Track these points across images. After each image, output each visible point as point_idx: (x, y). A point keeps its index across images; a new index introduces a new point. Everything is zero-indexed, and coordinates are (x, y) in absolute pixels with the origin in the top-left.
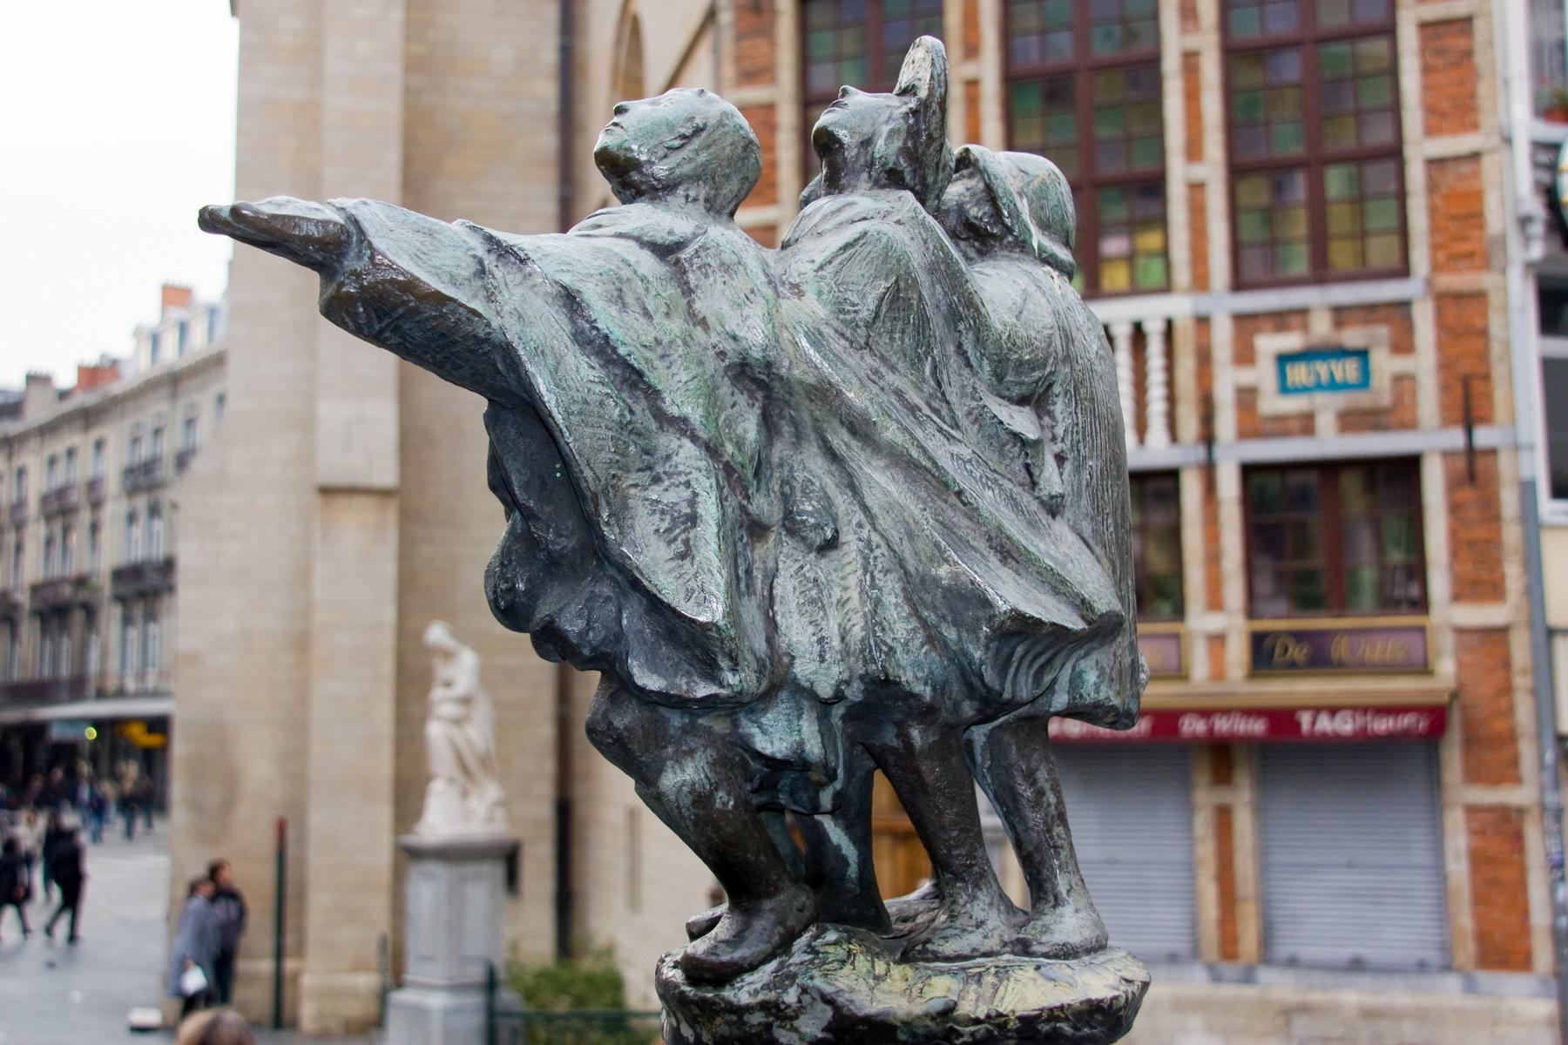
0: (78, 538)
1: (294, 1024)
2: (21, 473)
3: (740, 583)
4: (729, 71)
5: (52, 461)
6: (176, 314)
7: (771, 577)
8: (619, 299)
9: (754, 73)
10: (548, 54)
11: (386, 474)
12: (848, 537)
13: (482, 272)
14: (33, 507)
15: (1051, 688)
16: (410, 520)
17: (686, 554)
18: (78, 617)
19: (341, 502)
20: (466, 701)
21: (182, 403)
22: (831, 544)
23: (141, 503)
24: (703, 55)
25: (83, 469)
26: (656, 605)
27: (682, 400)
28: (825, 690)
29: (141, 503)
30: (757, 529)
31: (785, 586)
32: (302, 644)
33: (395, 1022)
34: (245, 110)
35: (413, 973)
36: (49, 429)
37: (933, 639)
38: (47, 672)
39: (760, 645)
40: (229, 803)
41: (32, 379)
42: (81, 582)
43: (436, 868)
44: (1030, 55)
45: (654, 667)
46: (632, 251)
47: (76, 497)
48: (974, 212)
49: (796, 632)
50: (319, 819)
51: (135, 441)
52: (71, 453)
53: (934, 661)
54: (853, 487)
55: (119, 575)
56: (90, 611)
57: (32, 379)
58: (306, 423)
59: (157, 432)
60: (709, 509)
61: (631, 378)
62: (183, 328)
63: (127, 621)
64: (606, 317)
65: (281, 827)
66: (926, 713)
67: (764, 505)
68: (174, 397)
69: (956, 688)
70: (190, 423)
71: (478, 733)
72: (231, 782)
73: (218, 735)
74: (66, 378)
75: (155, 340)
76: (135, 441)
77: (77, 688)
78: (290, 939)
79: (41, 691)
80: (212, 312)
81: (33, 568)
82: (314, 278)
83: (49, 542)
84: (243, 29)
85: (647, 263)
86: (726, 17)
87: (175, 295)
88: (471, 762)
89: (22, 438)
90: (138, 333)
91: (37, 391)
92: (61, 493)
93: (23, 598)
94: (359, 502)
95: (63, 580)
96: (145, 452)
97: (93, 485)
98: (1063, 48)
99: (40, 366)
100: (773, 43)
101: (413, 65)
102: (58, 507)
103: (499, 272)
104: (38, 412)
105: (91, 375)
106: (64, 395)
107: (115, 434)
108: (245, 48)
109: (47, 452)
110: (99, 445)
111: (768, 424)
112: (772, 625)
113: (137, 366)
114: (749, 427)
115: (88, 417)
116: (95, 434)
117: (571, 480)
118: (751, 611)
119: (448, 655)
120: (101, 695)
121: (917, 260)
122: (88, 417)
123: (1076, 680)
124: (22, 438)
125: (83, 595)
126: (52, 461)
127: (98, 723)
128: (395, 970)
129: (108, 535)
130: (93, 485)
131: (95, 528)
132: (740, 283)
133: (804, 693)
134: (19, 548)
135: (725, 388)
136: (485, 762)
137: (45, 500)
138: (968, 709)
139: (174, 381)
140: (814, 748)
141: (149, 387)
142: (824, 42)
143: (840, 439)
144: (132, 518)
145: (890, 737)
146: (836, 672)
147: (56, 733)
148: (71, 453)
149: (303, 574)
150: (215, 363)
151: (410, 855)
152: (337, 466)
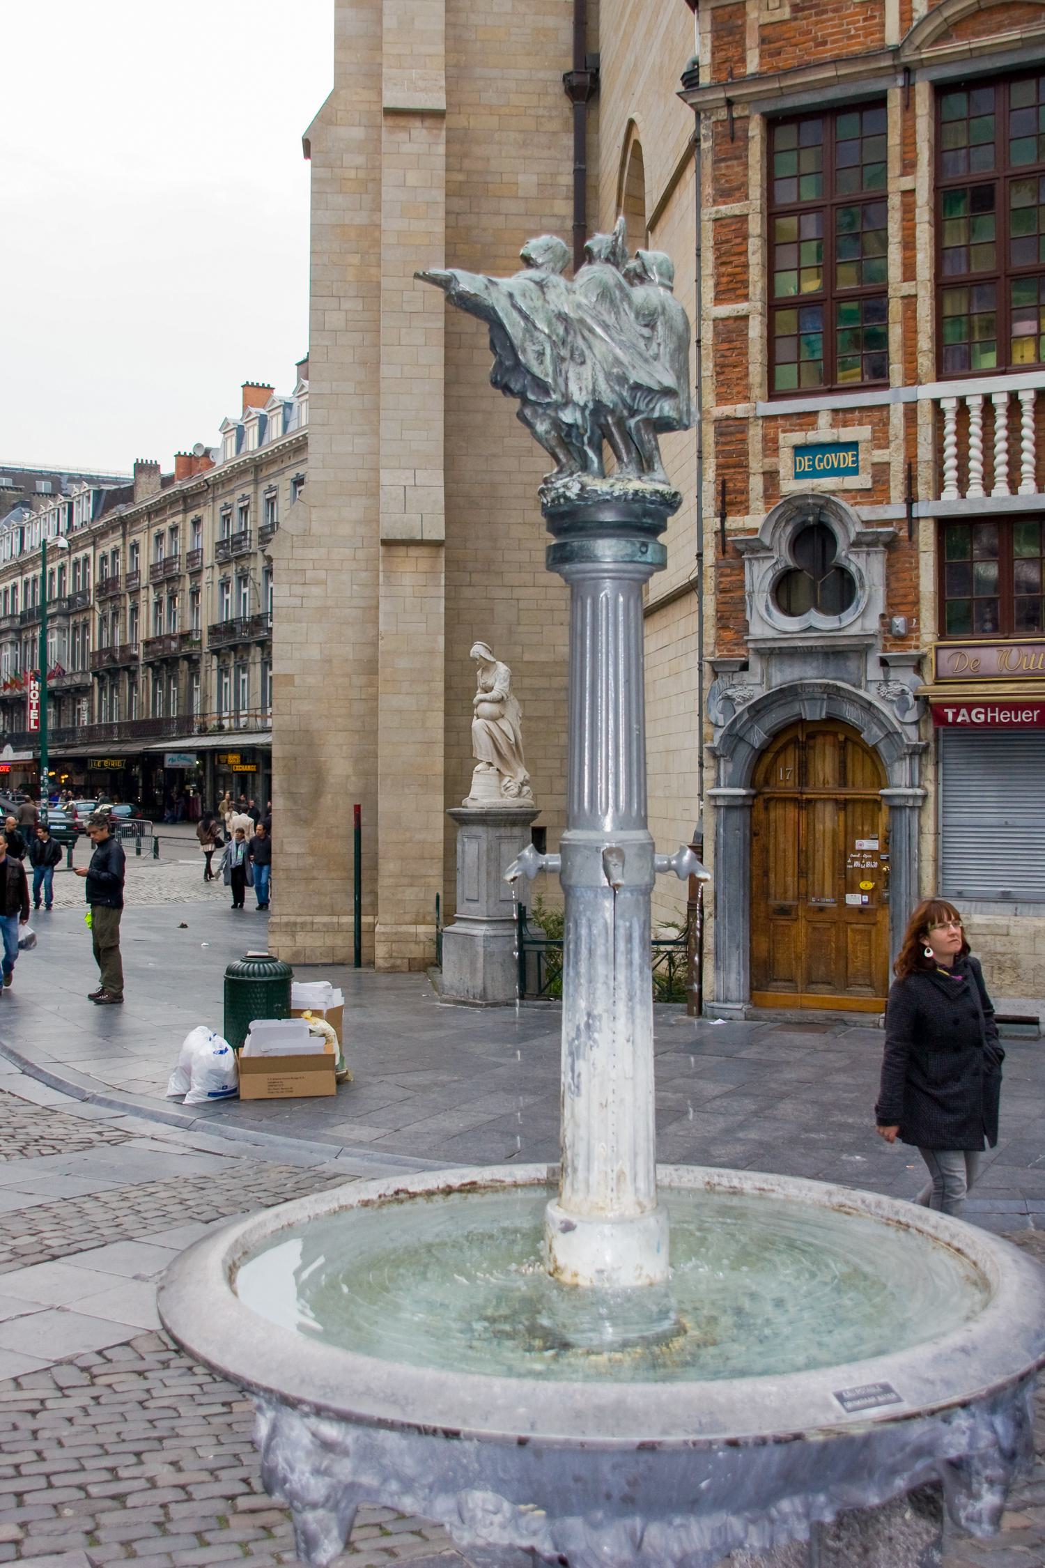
0: (183, 600)
1: (371, 963)
2: (135, 547)
3: (557, 372)
4: (708, 190)
5: (159, 537)
6: (256, 411)
7: (567, 372)
8: (524, 295)
9: (726, 193)
10: (567, 179)
11: (437, 532)
12: (589, 362)
13: (487, 288)
14: (144, 578)
15: (653, 409)
16: (453, 565)
17: (542, 363)
18: (184, 665)
19: (401, 551)
20: (500, 701)
21: (264, 486)
22: (583, 363)
23: (232, 571)
24: (690, 175)
25: (185, 543)
26: (534, 377)
27: (542, 325)
28: (582, 404)
29: (232, 571)
30: (563, 359)
31: (571, 375)
32: (371, 667)
33: (447, 946)
34: (318, 232)
35: (463, 910)
36: (155, 511)
37: (613, 390)
38: (159, 714)
39: (563, 389)
40: (317, 793)
41: (140, 467)
42: (185, 637)
43: (478, 830)
44: (959, 173)
45: (534, 393)
46: (528, 282)
47: (180, 567)
48: (639, 270)
49: (573, 388)
50: (386, 804)
51: (226, 518)
52: (174, 530)
53: (615, 398)
54: (590, 347)
55: (214, 630)
56: (193, 662)
57: (140, 467)
58: (373, 491)
59: (244, 510)
60: (548, 351)
61: (526, 317)
62: (263, 422)
63: (223, 671)
64: (521, 302)
65: (357, 809)
66: (612, 412)
67: (564, 352)
68: (256, 482)
69: (621, 406)
70: (271, 502)
71: (509, 726)
72: (318, 777)
73: (307, 740)
74: (168, 468)
75: (241, 433)
76: (226, 518)
77: (185, 725)
78: (365, 900)
79: (155, 728)
80: (288, 406)
81: (146, 629)
82: (441, 290)
83: (158, 604)
84: (313, 166)
85: (532, 285)
86: (706, 145)
87: (255, 393)
88: (505, 750)
89: (134, 519)
90: (225, 428)
91: (143, 478)
92: (168, 563)
93: (139, 652)
94: (414, 552)
95: (171, 637)
96: (234, 529)
97: (193, 556)
98: (983, 165)
99: (148, 456)
100: (746, 166)
101: (452, 192)
102: (165, 576)
103: (491, 288)
104: (147, 496)
105: (188, 463)
106: (167, 482)
107: (210, 514)
108: (314, 180)
109: (154, 530)
110: (197, 523)
111: (566, 330)
112: (567, 385)
113: (226, 455)
114: (561, 331)
115: (187, 500)
116: (191, 516)
117: (512, 346)
118: (561, 381)
119: (487, 666)
120: (204, 731)
121: (611, 282)
122: (187, 500)
123: (661, 409)
124: (134, 519)
125: (186, 649)
126: (159, 537)
127: (201, 753)
128: (446, 912)
129: (208, 597)
130: (193, 556)
131: (195, 593)
132: (558, 291)
133: (576, 404)
134: (135, 610)
135: (554, 320)
136: (515, 748)
137: (153, 570)
138: (626, 413)
139: (256, 468)
140: (580, 422)
141: (237, 472)
142: (786, 163)
143: (586, 333)
144: (225, 585)
145: (602, 420)
146: (585, 398)
147: (169, 761)
148: (174, 530)
149: (372, 611)
150: (299, 447)
151: (458, 820)
152: (396, 524)
